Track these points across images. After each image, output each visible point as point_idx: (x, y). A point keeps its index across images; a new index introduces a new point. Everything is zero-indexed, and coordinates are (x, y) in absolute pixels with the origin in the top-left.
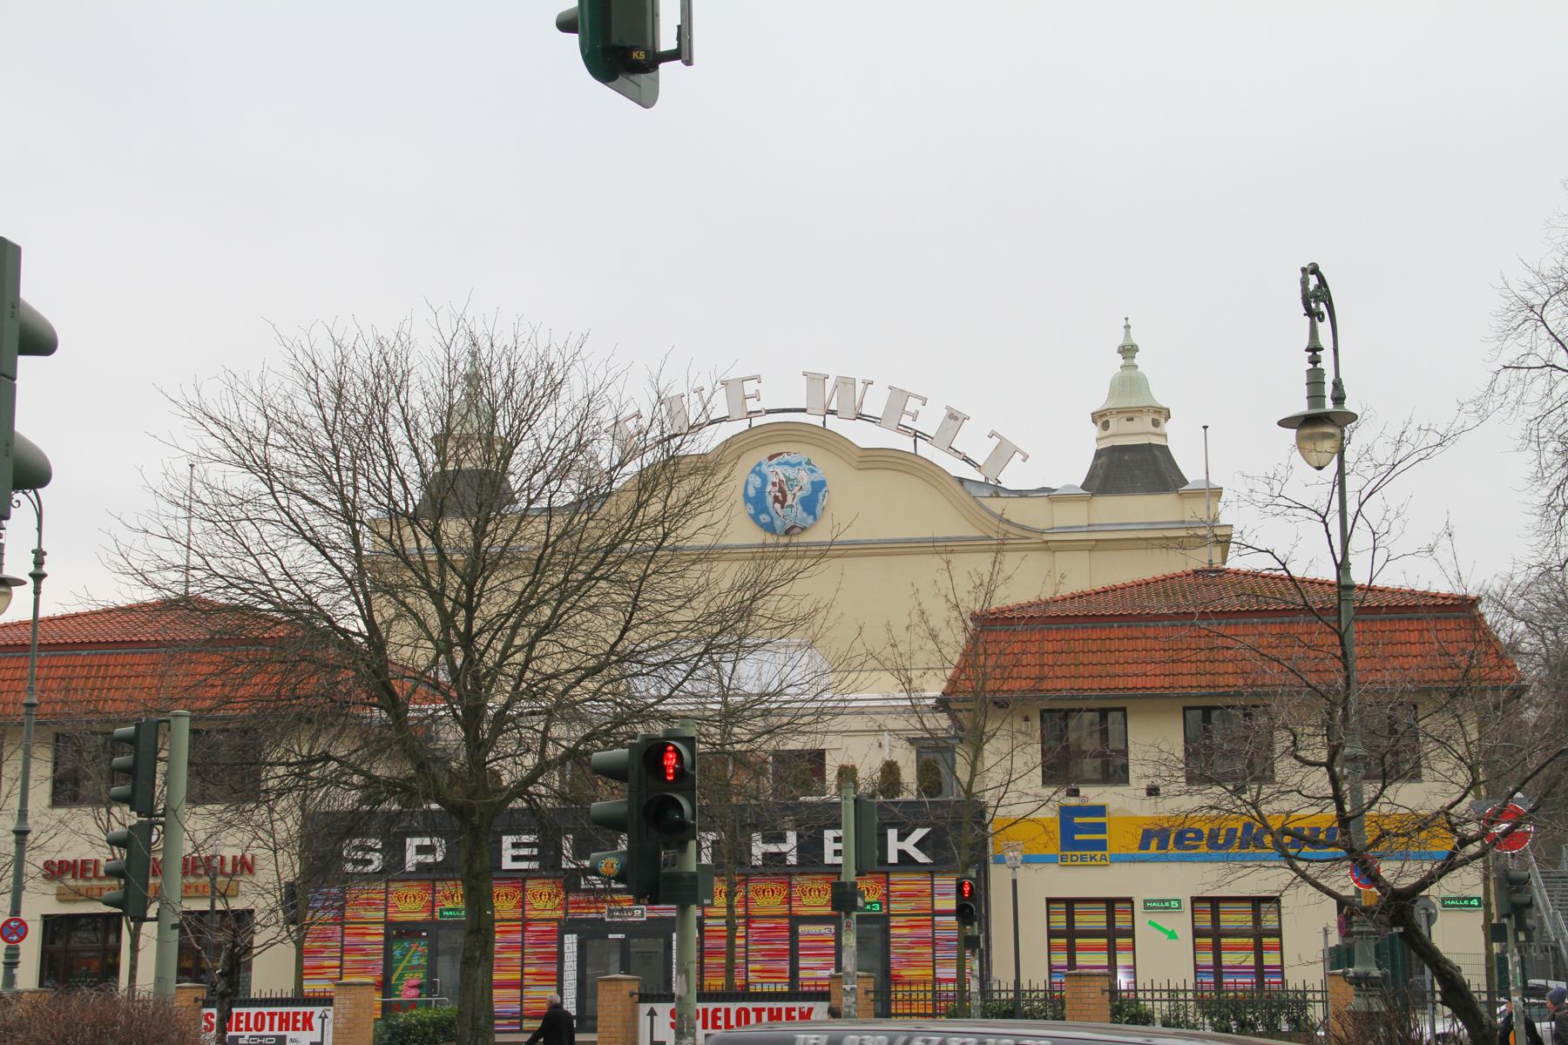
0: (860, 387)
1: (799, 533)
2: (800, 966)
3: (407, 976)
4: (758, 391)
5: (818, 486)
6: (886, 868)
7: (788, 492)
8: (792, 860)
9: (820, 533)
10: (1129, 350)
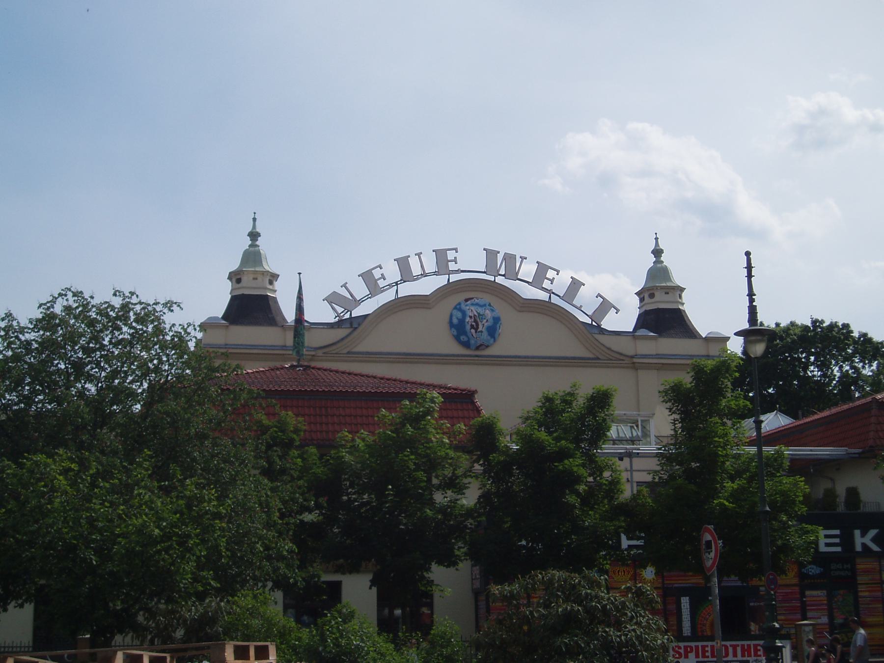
0: (518, 260)
1: (484, 349)
5: (497, 320)
7: (480, 323)
9: (495, 350)
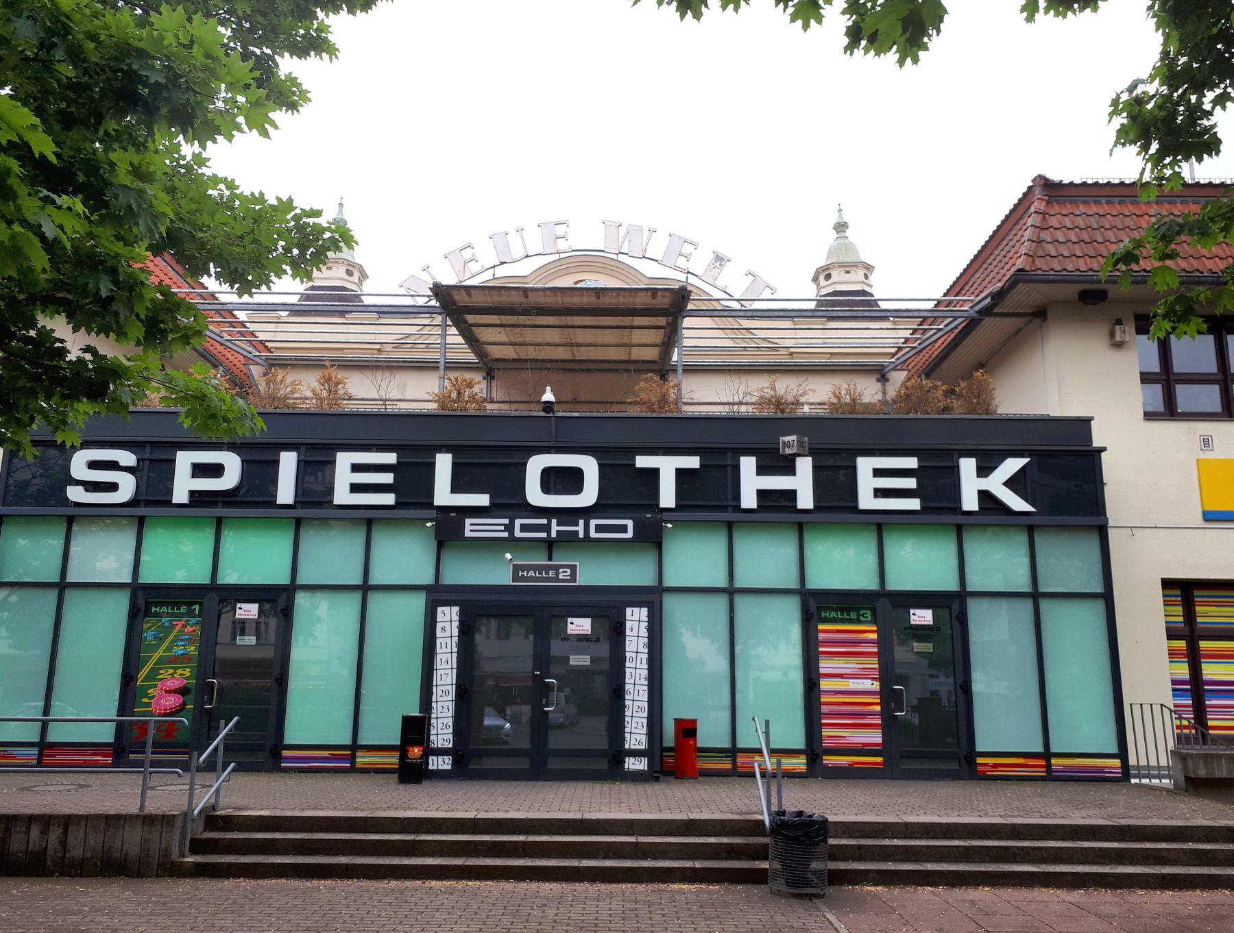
0: (646, 234)
2: (822, 671)
3: (163, 674)
4: (566, 232)
6: (960, 519)
8: (805, 501)
10: (843, 226)
